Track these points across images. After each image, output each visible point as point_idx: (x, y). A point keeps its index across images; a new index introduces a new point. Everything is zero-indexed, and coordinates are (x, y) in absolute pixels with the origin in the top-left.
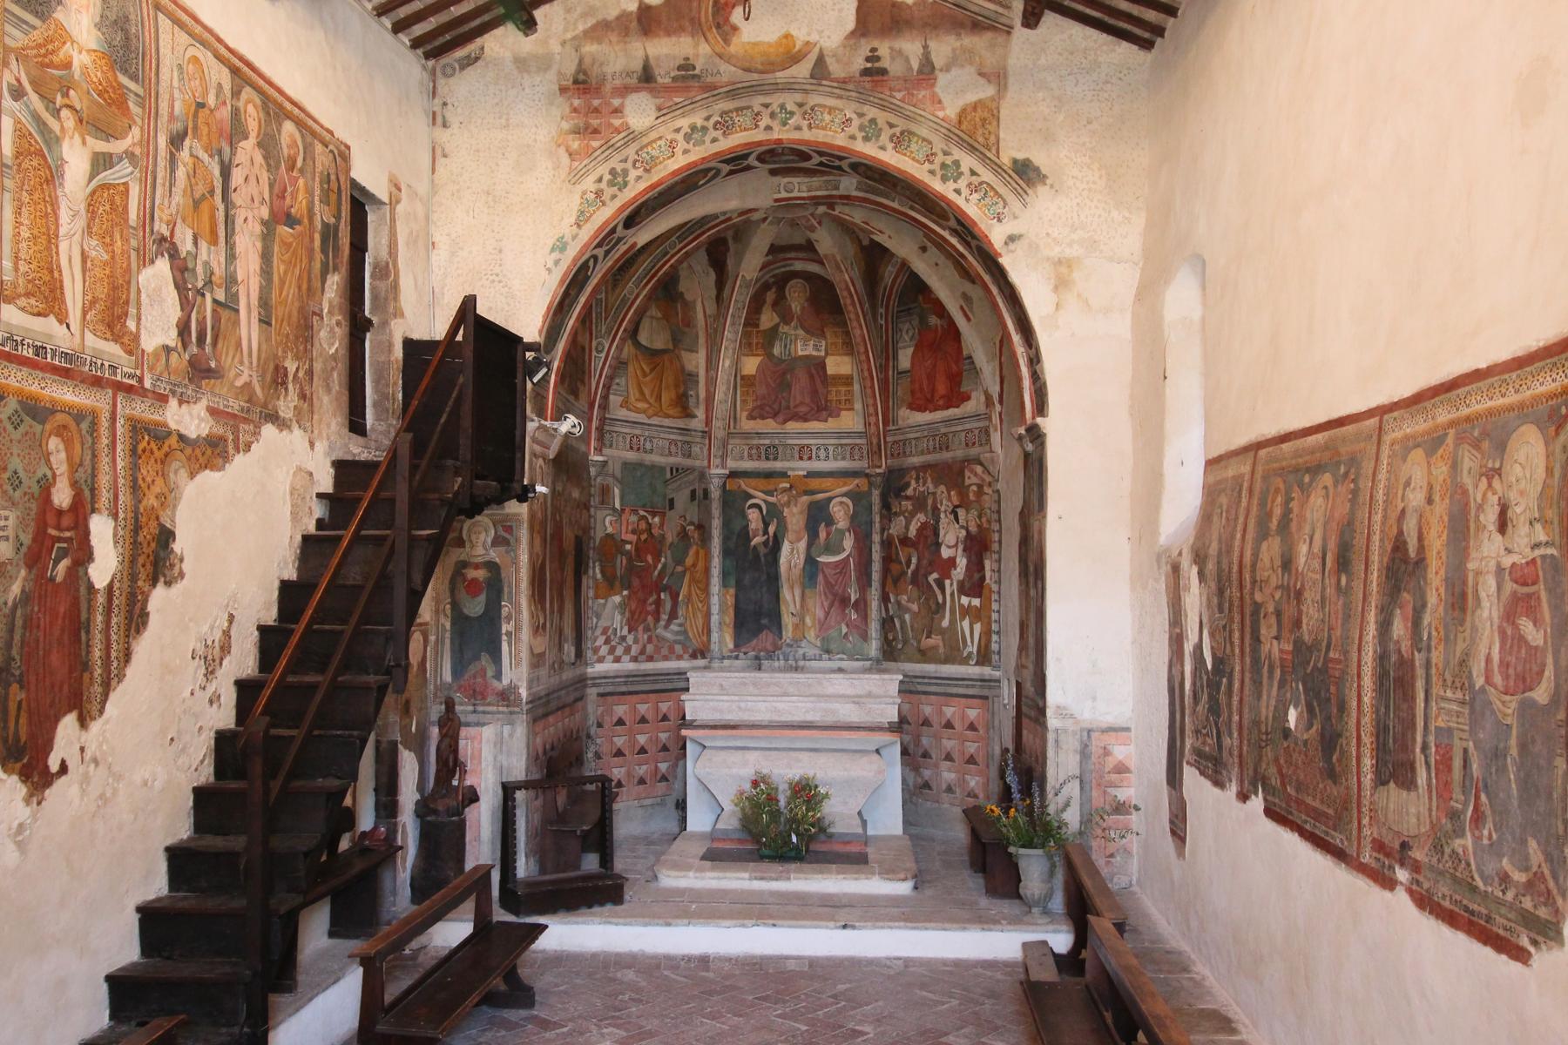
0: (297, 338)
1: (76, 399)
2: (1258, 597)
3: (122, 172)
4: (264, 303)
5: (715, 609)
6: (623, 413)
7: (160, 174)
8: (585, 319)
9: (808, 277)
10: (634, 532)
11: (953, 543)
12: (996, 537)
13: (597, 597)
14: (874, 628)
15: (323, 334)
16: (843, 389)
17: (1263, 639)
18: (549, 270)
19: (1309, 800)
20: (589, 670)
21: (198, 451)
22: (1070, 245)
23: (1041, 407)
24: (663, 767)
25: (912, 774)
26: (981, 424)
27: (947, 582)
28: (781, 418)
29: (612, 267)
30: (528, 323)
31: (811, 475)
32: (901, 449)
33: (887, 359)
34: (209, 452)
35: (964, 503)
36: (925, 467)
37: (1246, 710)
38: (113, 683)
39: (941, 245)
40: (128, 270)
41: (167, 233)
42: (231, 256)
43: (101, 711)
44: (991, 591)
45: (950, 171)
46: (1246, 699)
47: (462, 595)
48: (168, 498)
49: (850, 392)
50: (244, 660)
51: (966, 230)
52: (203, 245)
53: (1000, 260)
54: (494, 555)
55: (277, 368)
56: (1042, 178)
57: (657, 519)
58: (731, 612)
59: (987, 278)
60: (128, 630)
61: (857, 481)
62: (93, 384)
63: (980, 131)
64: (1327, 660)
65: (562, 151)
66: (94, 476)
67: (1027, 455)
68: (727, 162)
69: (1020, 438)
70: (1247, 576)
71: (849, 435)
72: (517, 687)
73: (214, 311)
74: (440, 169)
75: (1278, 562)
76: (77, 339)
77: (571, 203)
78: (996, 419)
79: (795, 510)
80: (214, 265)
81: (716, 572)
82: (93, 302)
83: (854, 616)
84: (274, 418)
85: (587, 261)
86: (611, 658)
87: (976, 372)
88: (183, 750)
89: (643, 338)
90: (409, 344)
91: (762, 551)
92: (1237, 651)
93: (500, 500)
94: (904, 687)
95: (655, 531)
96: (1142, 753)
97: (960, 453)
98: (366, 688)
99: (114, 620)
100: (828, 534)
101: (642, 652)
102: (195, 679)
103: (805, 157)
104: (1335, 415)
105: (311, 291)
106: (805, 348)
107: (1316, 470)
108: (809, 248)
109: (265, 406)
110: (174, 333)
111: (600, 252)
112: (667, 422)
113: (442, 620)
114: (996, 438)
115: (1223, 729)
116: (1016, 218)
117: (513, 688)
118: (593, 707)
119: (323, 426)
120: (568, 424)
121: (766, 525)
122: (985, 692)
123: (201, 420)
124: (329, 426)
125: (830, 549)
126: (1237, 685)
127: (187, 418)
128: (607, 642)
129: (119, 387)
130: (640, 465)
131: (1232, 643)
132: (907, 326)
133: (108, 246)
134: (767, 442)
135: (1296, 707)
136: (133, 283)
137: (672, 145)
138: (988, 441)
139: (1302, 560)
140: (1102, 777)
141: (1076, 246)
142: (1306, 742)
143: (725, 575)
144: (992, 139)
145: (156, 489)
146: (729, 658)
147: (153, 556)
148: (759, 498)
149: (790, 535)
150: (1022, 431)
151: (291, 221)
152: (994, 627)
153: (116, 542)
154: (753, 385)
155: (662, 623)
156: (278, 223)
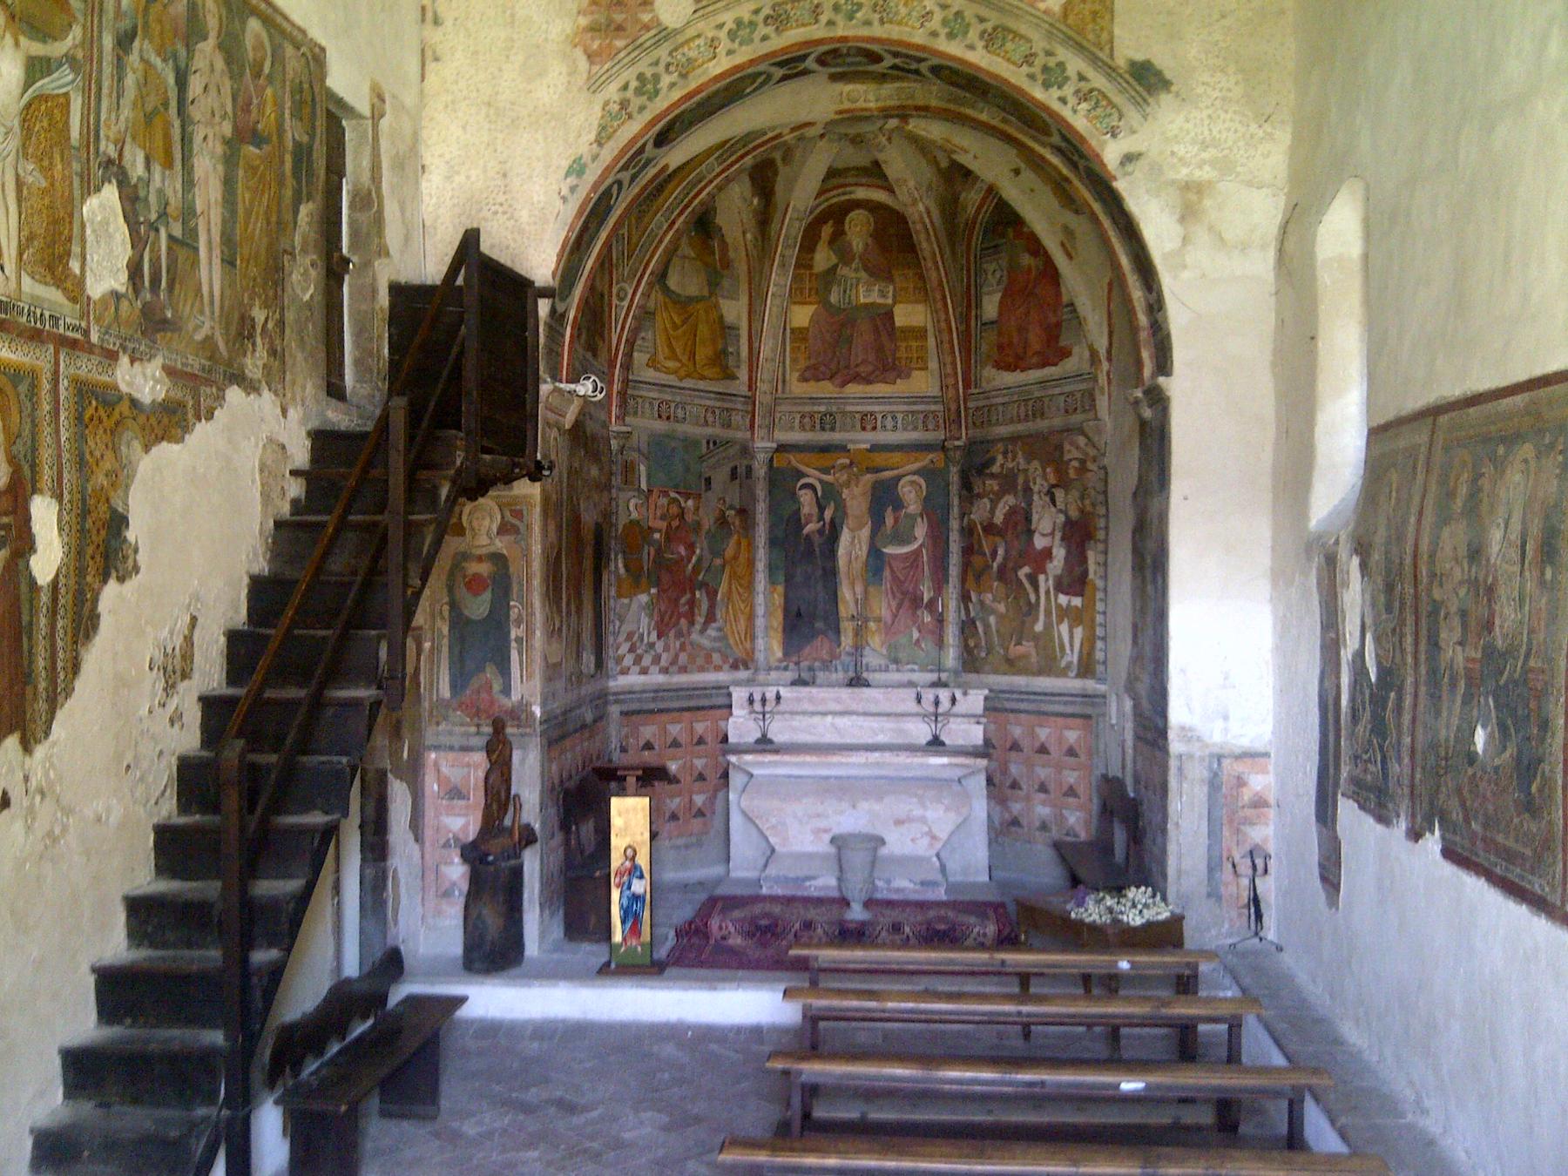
0: (266, 283)
1: (12, 356)
2: (1437, 594)
3: (61, 81)
4: (228, 240)
5: (760, 611)
6: (650, 375)
7: (106, 84)
8: (605, 263)
9: (873, 207)
10: (663, 518)
11: (1048, 530)
12: (1102, 523)
13: (620, 595)
14: (951, 634)
15: (295, 277)
16: (914, 344)
17: (1442, 644)
18: (564, 199)
19: (1500, 838)
20: (612, 684)
21: (153, 421)
22: (1200, 167)
23: (1164, 365)
24: (699, 800)
25: (998, 808)
26: (1083, 386)
27: (1042, 578)
28: (838, 380)
29: (639, 195)
30: (539, 261)
31: (875, 448)
32: (984, 416)
33: (969, 306)
34: (166, 420)
35: (1063, 483)
36: (1013, 439)
37: (1420, 731)
38: (60, 699)
39: (1038, 164)
40: (71, 199)
41: (114, 154)
42: (189, 183)
43: (47, 734)
44: (1095, 589)
45: (1053, 76)
46: (1420, 717)
47: (462, 592)
48: (121, 477)
49: (923, 348)
50: (210, 673)
51: (1075, 151)
52: (157, 170)
53: (1116, 184)
54: (500, 545)
55: (242, 318)
56: (1166, 84)
57: (690, 503)
58: (779, 614)
59: (1097, 207)
60: (75, 635)
61: (931, 456)
62: (32, 338)
63: (1090, 26)
64: (1526, 671)
65: (579, 53)
66: (34, 449)
67: (1143, 424)
68: (780, 64)
69: (1137, 402)
70: (1424, 570)
71: (922, 399)
72: (529, 704)
73: (169, 249)
74: (431, 79)
75: (1463, 551)
76: (13, 284)
77: (585, 118)
78: (1103, 379)
79: (857, 491)
80: (169, 192)
81: (761, 565)
82: (31, 238)
83: (928, 619)
84: (239, 379)
85: (611, 186)
86: (637, 669)
87: (1079, 321)
88: (142, 779)
89: (673, 282)
90: (396, 290)
91: (817, 540)
92: (1409, 659)
93: (508, 480)
94: (990, 704)
95: (689, 517)
96: (1284, 780)
97: (1058, 422)
98: (355, 703)
99: (60, 624)
100: (896, 520)
101: (674, 662)
102: (154, 695)
103: (875, 58)
104: (1538, 371)
105: (280, 226)
106: (869, 294)
107: (1512, 439)
108: (875, 173)
109: (229, 364)
110: (124, 276)
111: (625, 176)
112: (702, 385)
113: (439, 623)
114: (1102, 403)
115: (1391, 753)
116: (1134, 132)
117: (524, 706)
118: (615, 731)
119: (298, 389)
120: (585, 388)
121: (821, 509)
122: (1089, 710)
123: (157, 381)
124: (304, 388)
125: (901, 538)
126: (1408, 701)
127: (139, 380)
128: (631, 650)
129: (64, 343)
130: (669, 436)
131: (1403, 651)
132: (991, 267)
133: (47, 171)
134: (823, 409)
135: (1484, 727)
136: (76, 216)
137: (713, 43)
138: (1093, 406)
139: (1495, 549)
140: (1234, 812)
141: (1207, 168)
142: (1496, 769)
143: (771, 569)
144: (1105, 36)
145: (107, 465)
146: (777, 668)
147: (103, 546)
148: (813, 477)
149: (850, 521)
150: (1139, 394)
151: (257, 139)
152: (1099, 631)
153: (60, 529)
154: (805, 339)
155: (698, 627)
156: (242, 141)
